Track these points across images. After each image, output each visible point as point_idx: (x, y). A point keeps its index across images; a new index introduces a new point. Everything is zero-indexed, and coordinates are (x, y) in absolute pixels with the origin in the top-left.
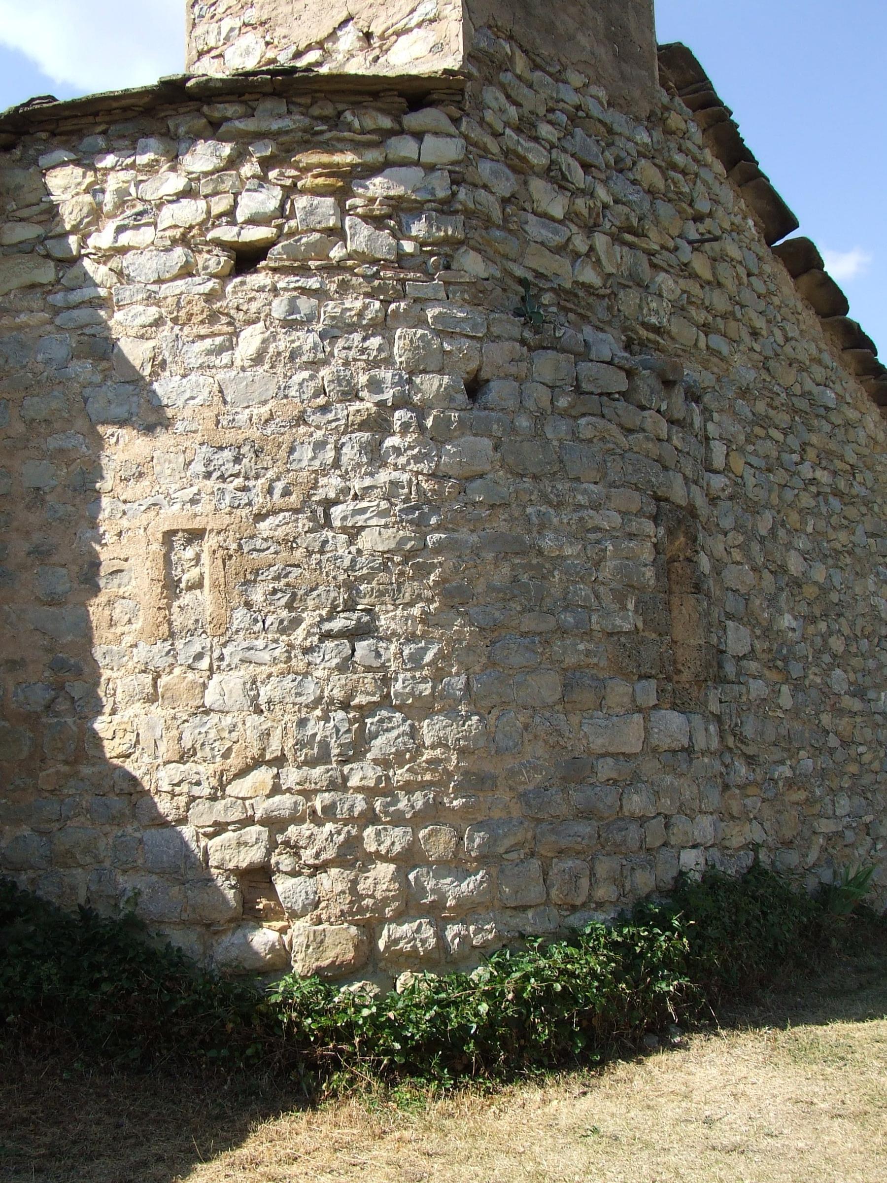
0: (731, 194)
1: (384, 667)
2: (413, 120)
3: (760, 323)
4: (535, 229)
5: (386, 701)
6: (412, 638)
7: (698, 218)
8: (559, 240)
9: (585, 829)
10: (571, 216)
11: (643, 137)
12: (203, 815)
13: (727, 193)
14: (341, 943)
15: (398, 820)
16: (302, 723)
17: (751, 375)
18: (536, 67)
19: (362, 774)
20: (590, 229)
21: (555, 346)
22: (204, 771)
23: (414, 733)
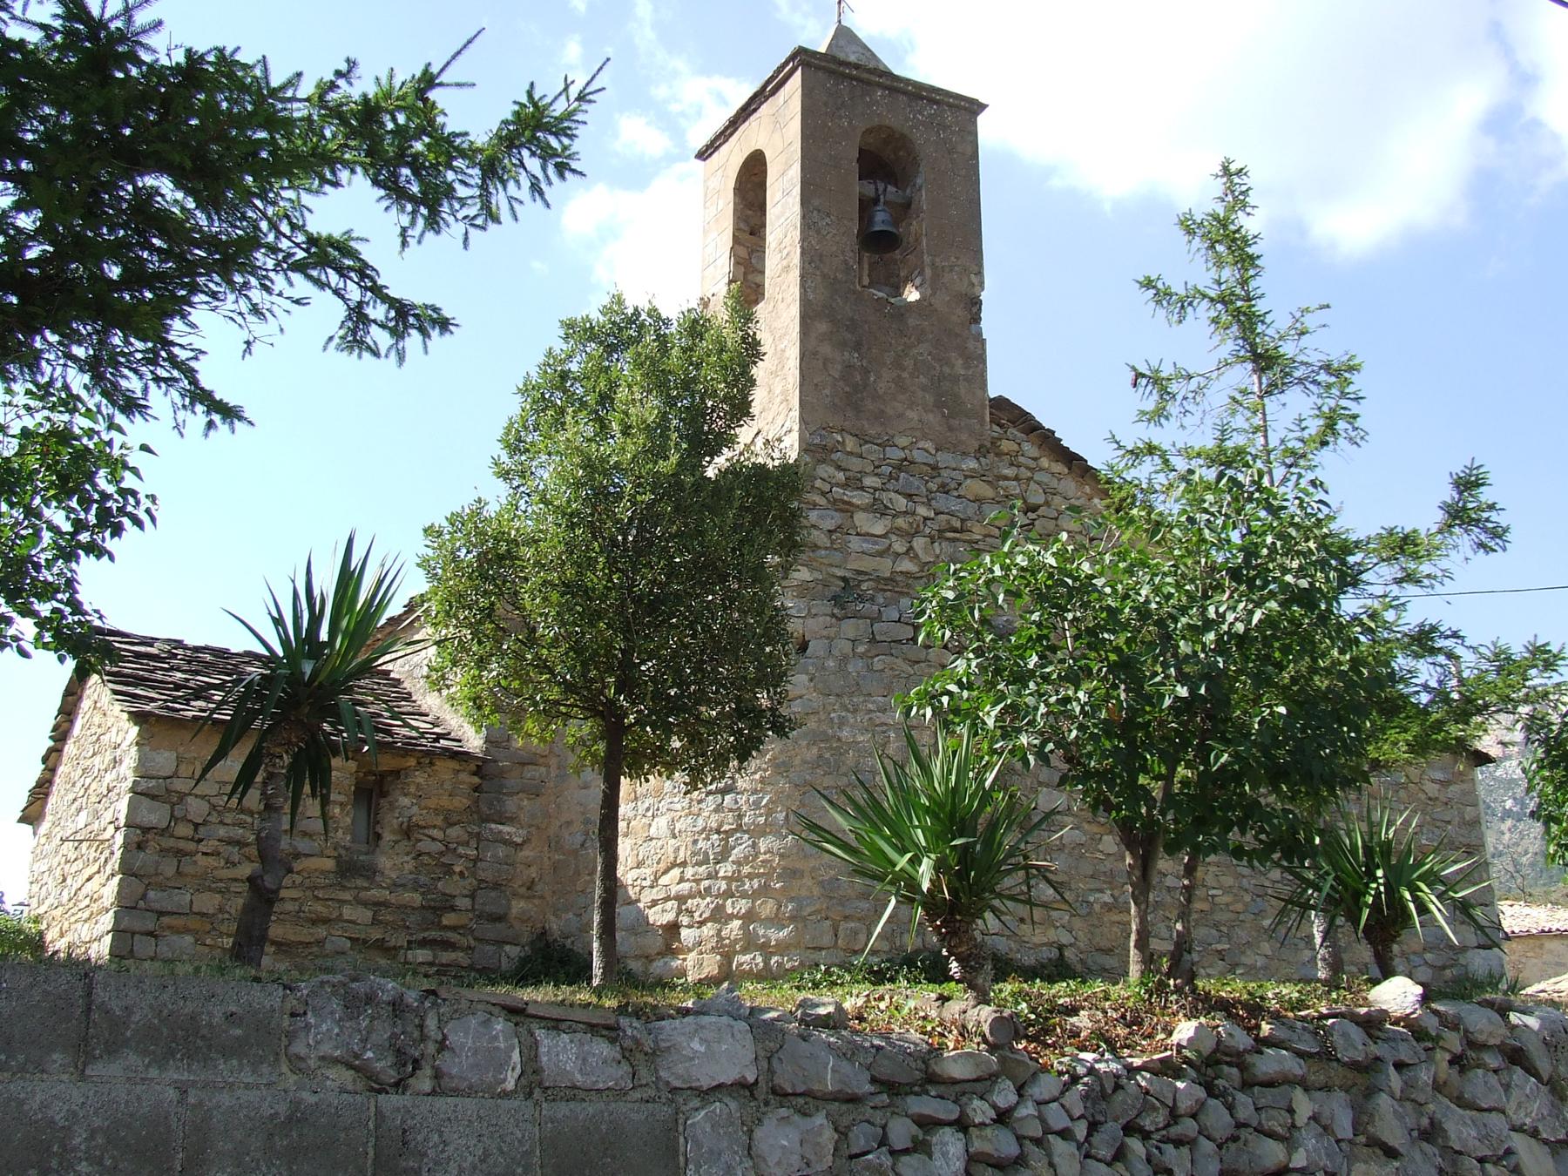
0: (1073, 485)
1: (739, 809)
5: (739, 828)
6: (755, 792)
12: (647, 897)
14: (711, 965)
15: (744, 895)
16: (695, 842)
19: (726, 869)
20: (909, 535)
21: (856, 616)
22: (647, 872)
23: (754, 845)
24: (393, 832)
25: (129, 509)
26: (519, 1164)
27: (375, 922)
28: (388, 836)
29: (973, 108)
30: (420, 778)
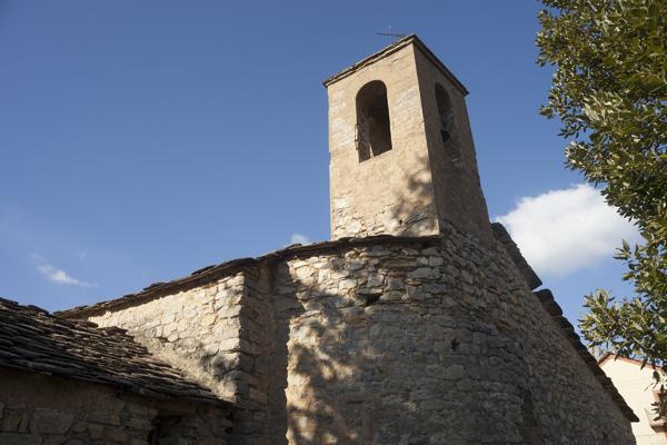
2: (425, 252)
3: (534, 319)
4: (466, 288)
7: (510, 281)
8: (472, 292)
10: (475, 283)
13: (517, 272)
17: (535, 339)
18: (458, 232)
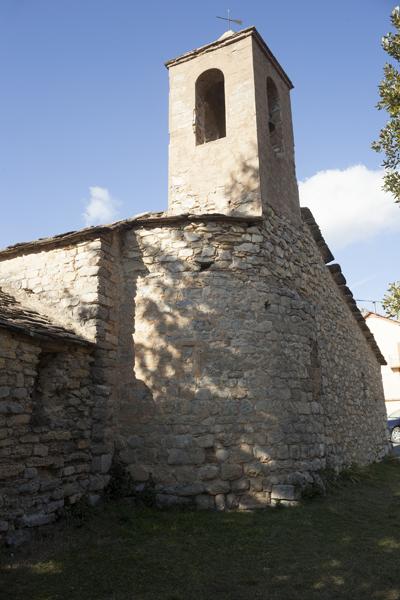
2: (249, 230)
4: (278, 261)
9: (298, 436)
11: (298, 233)
13: (316, 249)
24: (51, 392)
25: (309, 394)
26: (357, 453)
27: (52, 454)
28: (47, 394)
29: (223, 134)
30: (69, 358)
